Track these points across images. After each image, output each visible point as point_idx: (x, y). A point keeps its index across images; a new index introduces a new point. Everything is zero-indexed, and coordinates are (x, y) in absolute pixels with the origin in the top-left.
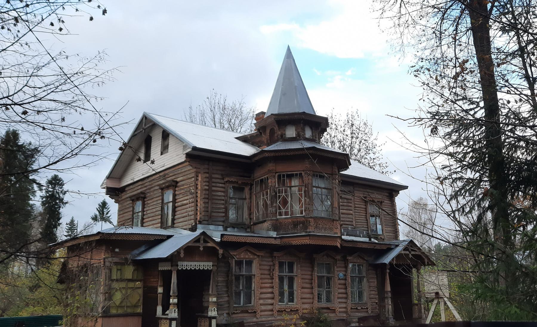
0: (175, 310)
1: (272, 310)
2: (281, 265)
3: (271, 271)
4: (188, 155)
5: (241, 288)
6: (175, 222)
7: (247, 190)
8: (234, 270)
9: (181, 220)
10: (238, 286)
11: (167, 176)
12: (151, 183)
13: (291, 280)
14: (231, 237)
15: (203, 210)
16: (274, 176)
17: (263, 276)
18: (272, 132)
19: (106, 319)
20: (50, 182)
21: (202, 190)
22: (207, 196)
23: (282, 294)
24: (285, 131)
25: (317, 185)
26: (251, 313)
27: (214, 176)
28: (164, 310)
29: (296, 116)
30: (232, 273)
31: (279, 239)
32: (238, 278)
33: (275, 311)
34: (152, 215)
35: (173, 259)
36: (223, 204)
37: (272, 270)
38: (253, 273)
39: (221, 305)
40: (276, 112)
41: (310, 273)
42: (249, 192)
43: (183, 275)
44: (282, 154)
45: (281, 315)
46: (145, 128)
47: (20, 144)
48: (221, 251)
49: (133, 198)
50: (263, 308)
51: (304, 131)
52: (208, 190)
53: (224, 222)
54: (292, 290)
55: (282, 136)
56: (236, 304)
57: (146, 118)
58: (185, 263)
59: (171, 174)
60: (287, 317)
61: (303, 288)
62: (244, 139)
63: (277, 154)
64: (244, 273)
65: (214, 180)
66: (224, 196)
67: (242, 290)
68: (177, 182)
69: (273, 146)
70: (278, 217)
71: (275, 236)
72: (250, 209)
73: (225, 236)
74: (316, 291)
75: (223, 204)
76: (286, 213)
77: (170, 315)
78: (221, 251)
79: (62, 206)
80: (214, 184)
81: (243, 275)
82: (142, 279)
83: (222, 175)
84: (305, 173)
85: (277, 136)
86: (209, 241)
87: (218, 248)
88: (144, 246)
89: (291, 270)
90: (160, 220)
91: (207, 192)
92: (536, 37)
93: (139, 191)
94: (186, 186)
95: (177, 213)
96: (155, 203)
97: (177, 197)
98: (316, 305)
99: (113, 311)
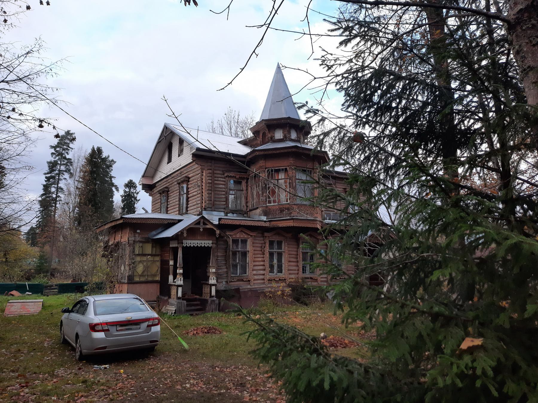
0: (181, 279)
1: (264, 279)
2: (271, 243)
3: (263, 248)
4: (194, 155)
5: (237, 261)
6: (188, 209)
7: (244, 183)
8: (231, 246)
9: (193, 208)
10: (235, 260)
11: (182, 173)
12: (172, 179)
13: (280, 255)
14: (227, 220)
15: (207, 199)
16: (264, 171)
17: (256, 252)
18: (264, 134)
19: (131, 285)
20: (127, 186)
21: (206, 183)
22: (210, 188)
23: (272, 267)
24: (274, 133)
25: (300, 178)
26: (246, 281)
27: (215, 172)
28: (175, 278)
29: (282, 121)
30: (229, 249)
31: (269, 223)
32: (234, 253)
33: (266, 280)
34: (173, 204)
35: (177, 237)
36: (224, 195)
37: (263, 247)
38: (248, 250)
39: (221, 275)
40: (267, 118)
41: (295, 250)
42: (246, 184)
43: (186, 250)
44: (270, 152)
45: (271, 283)
46: (166, 135)
47: (103, 157)
48: (218, 232)
49: (160, 192)
50: (256, 277)
51: (289, 133)
52: (211, 183)
53: (225, 209)
54: (280, 263)
55: (271, 138)
56: (233, 274)
57: (166, 128)
58: (189, 241)
59: (185, 172)
60: (274, 285)
61: (289, 262)
62: (244, 143)
63: (266, 153)
64: (240, 250)
65: (216, 175)
66: (225, 188)
67: (238, 263)
68: (189, 178)
69: (262, 146)
70: (268, 204)
71: (265, 220)
72: (246, 198)
73: (222, 220)
74: (301, 264)
75: (224, 195)
76: (274, 201)
77: (177, 282)
78: (218, 232)
79: (136, 202)
80: (216, 179)
81: (239, 251)
82: (160, 254)
83: (223, 171)
84: (290, 168)
85: (268, 139)
86: (208, 223)
87: (216, 229)
88: (160, 228)
89: (280, 247)
90: (178, 209)
91: (211, 185)
92: (492, 2)
93: (165, 186)
94: (195, 181)
95: (189, 203)
96: (175, 195)
97: (189, 190)
98: (301, 275)
99: (137, 279)
